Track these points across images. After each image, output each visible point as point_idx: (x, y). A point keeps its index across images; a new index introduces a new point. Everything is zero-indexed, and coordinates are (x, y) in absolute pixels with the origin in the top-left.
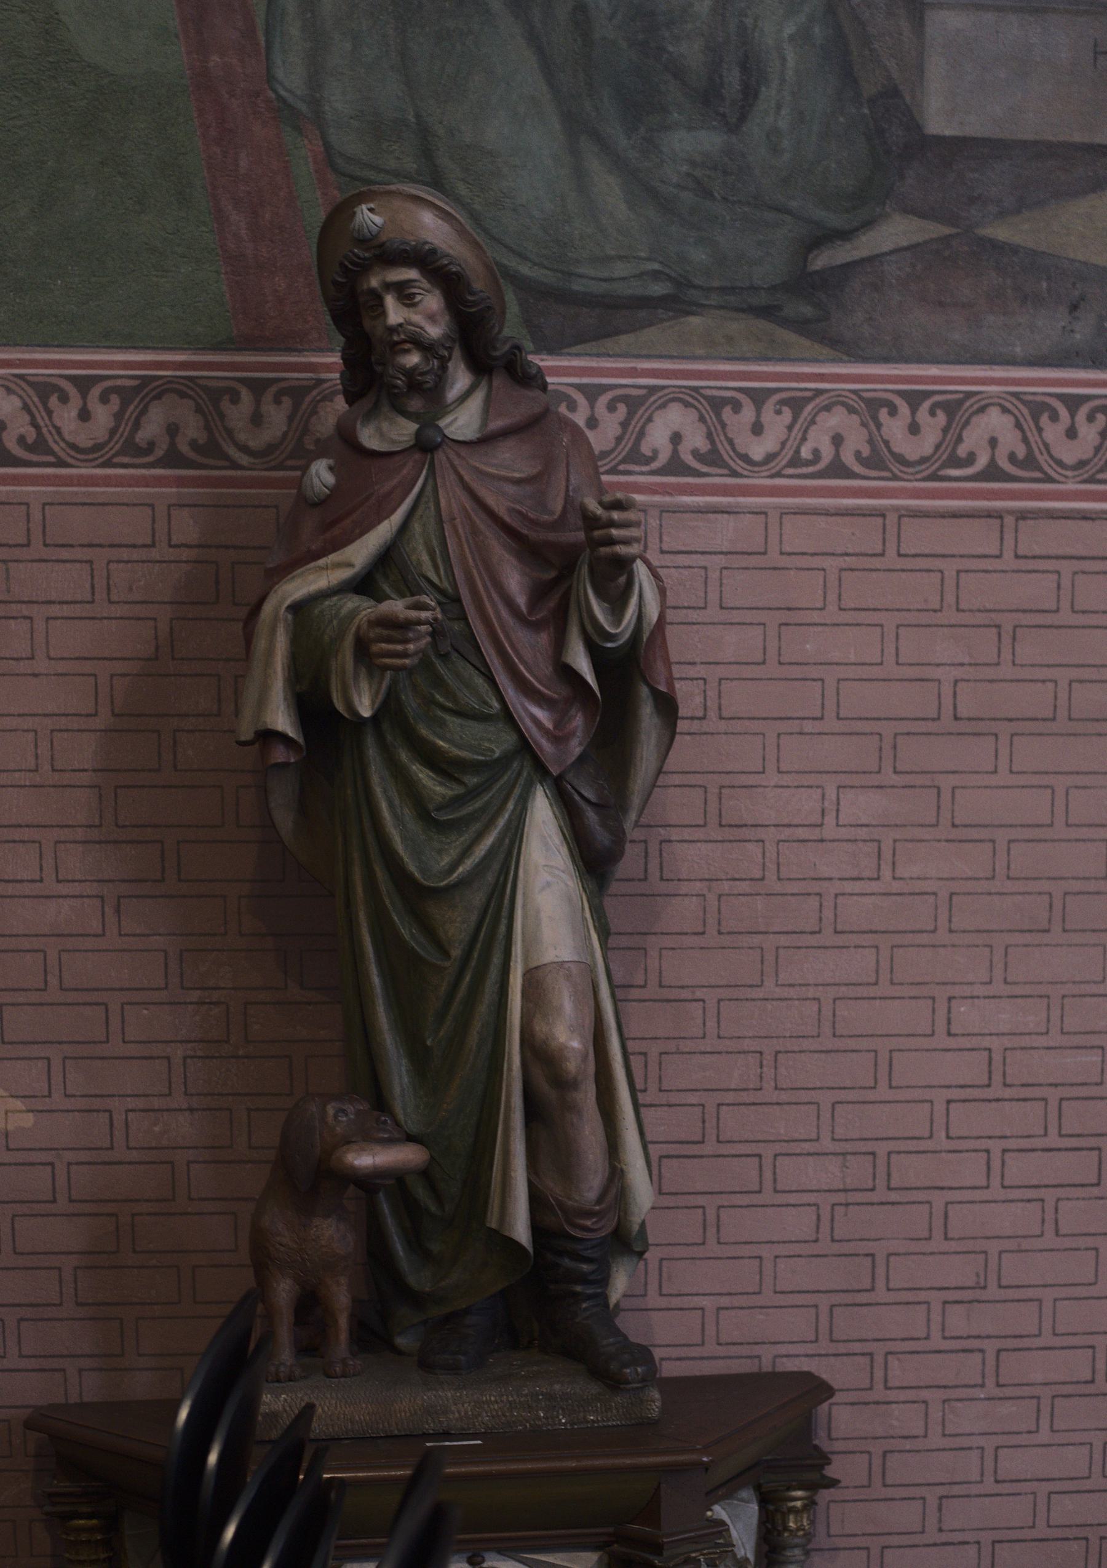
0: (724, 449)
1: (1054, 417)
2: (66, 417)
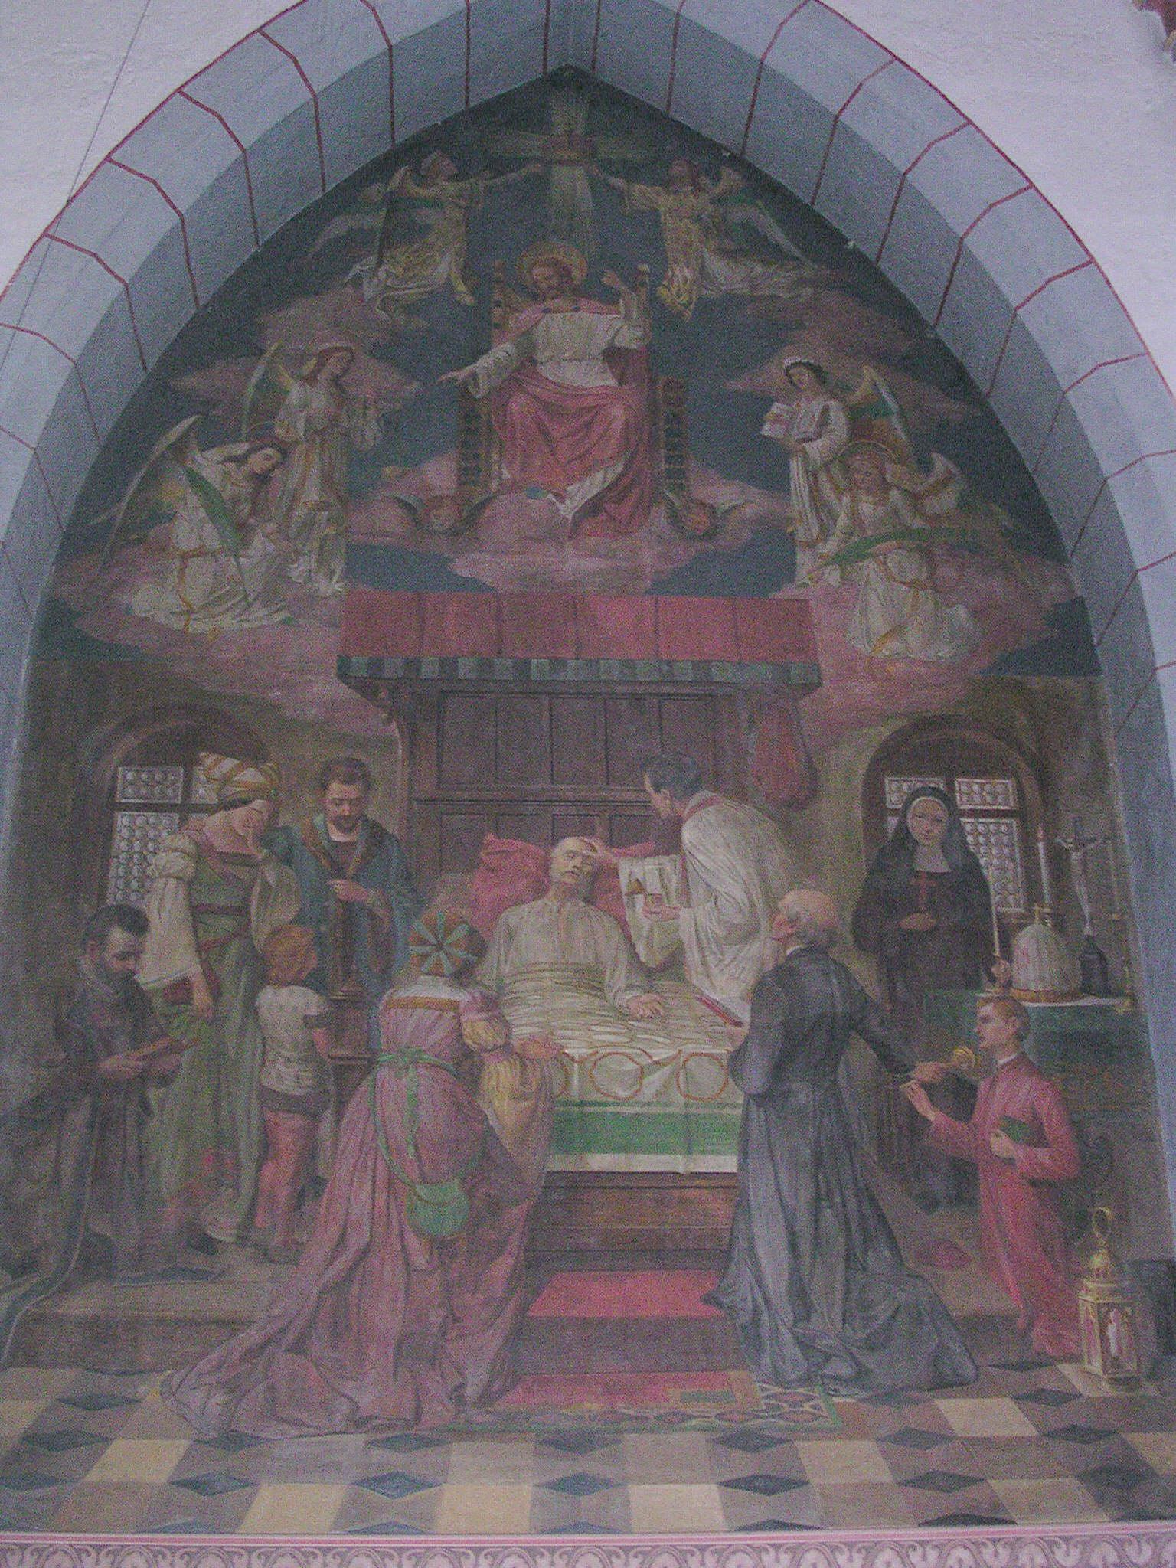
1: (164, 1556)
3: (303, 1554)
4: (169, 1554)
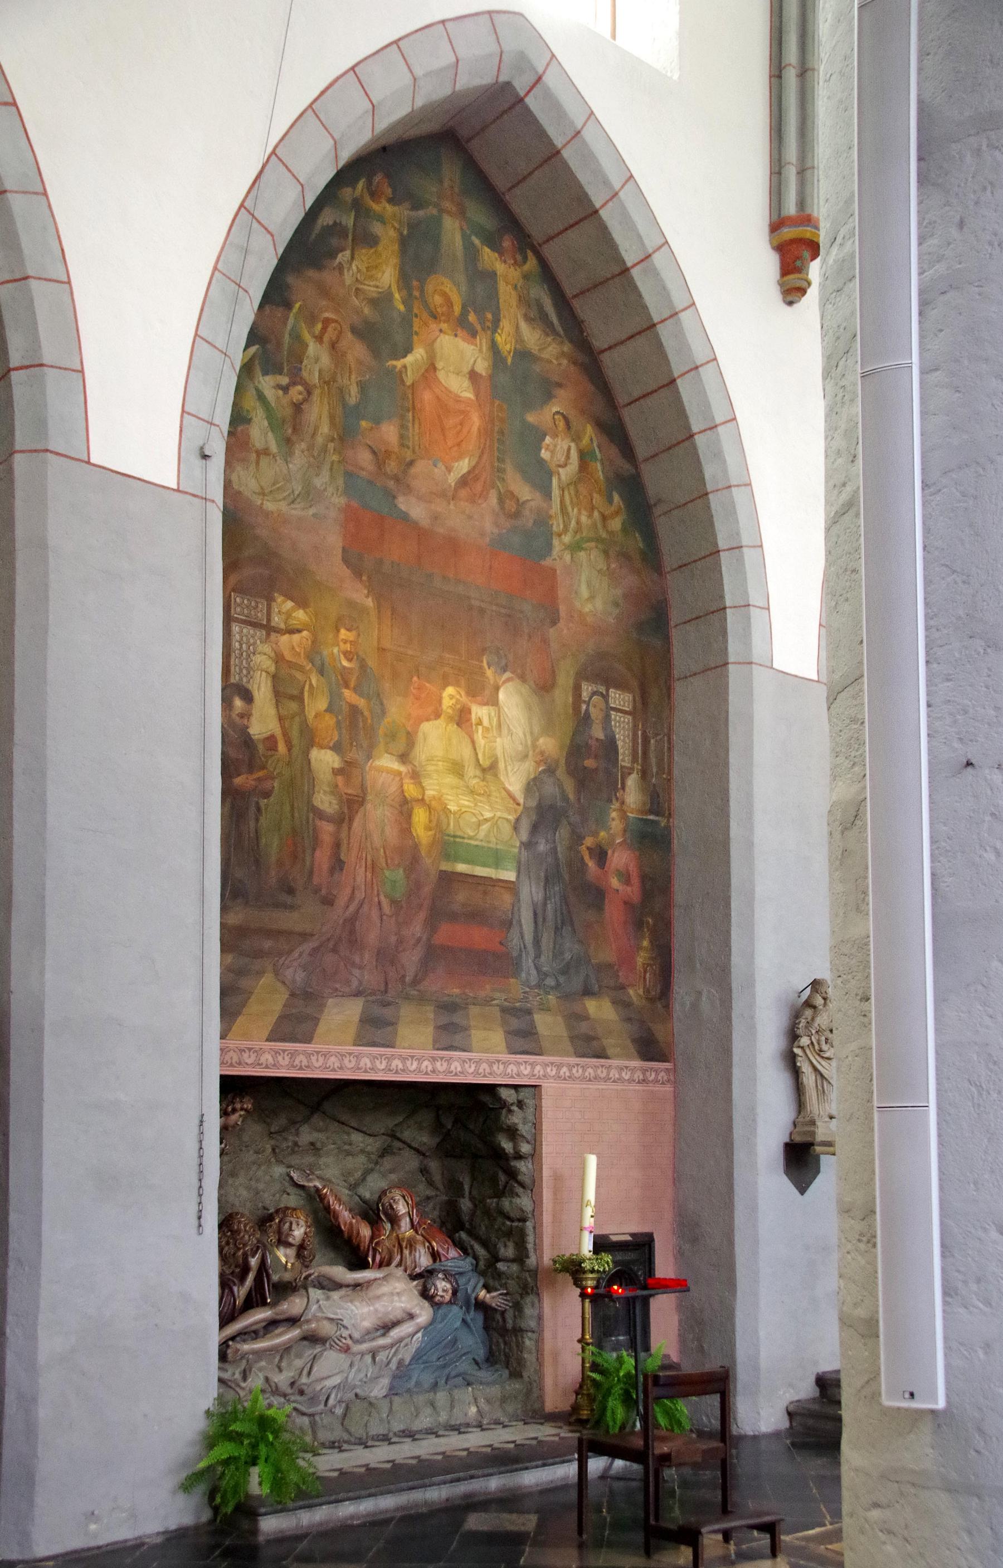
1: (280, 1054)
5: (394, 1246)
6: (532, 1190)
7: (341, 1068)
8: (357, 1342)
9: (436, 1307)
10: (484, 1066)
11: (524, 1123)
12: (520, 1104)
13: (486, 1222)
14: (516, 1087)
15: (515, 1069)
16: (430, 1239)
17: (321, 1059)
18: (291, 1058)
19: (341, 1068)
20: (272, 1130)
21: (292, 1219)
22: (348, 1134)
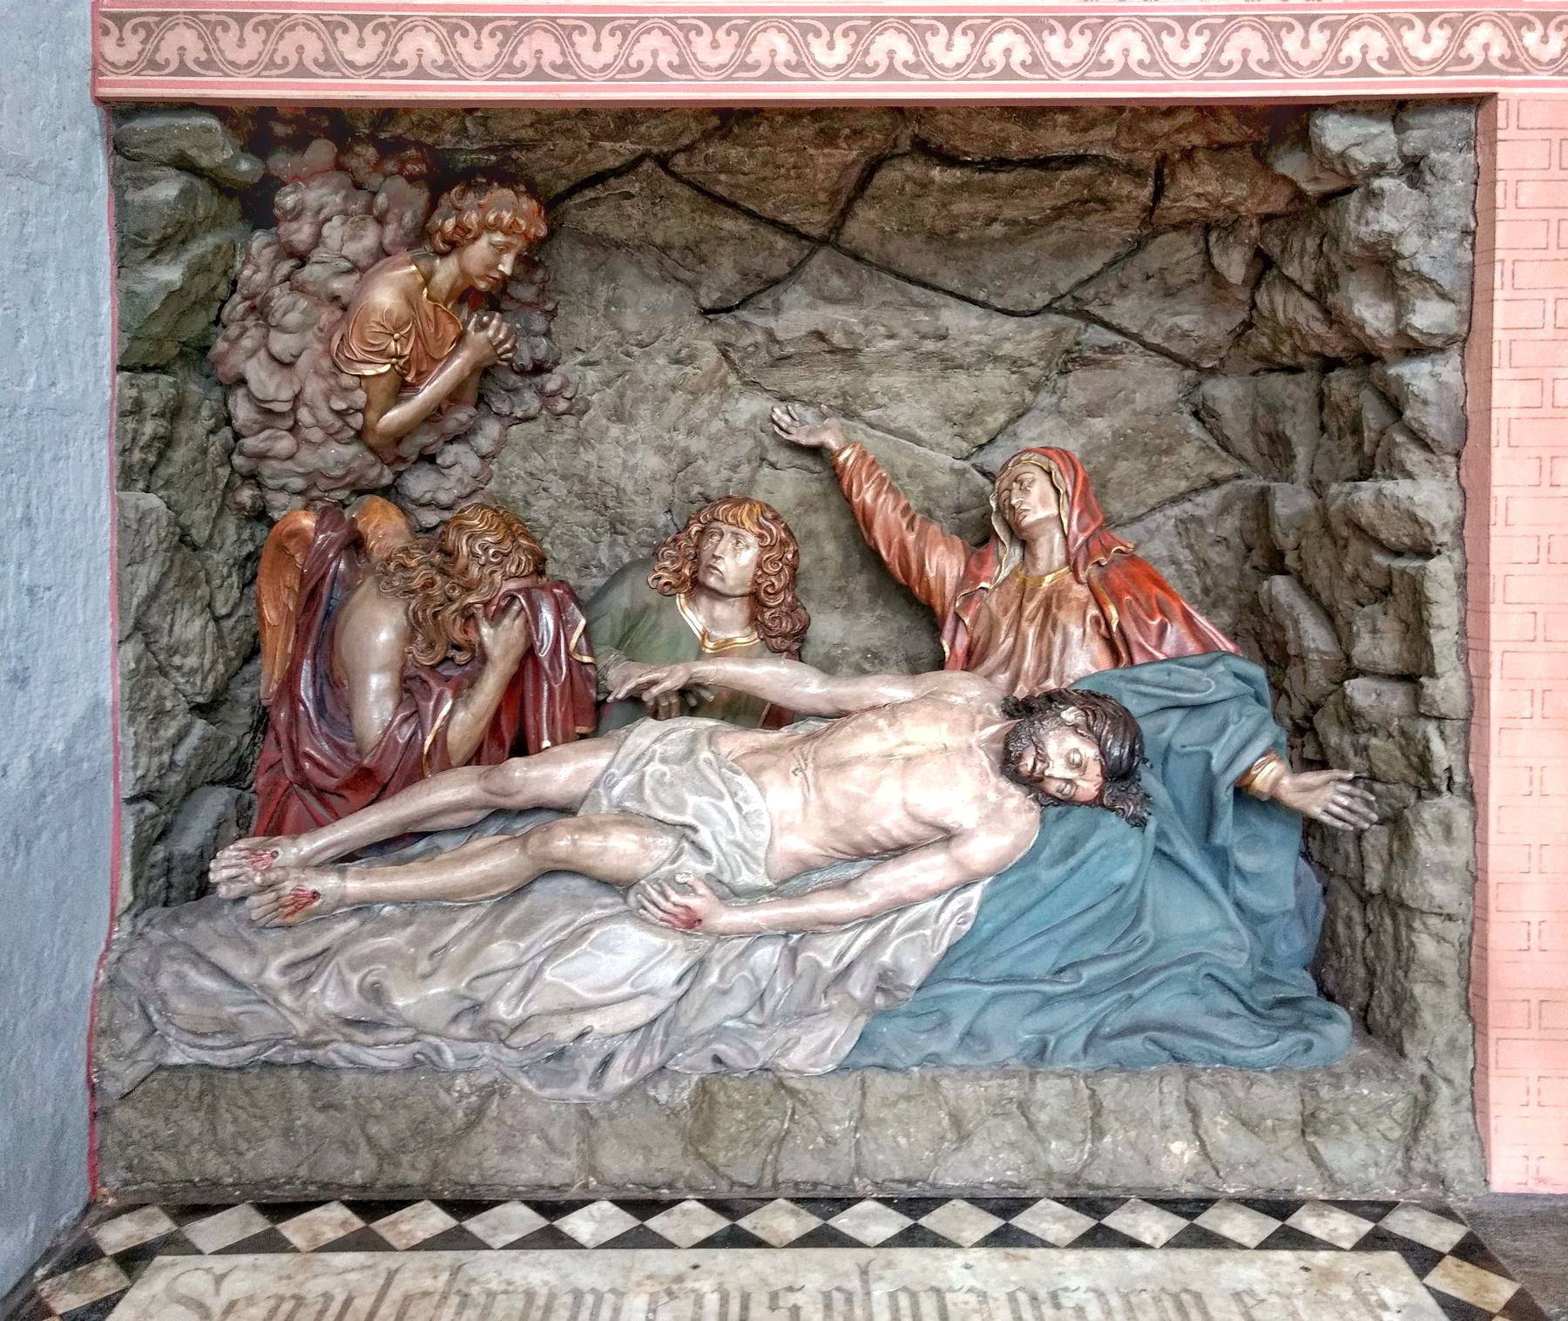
0: (690, 61)
1: (465, 34)
2: (313, 48)
3: (681, 27)
4: (234, 25)
5: (1006, 611)
6: (1458, 455)
7: (682, 68)
8: (732, 895)
9: (1053, 811)
10: (1248, 39)
11: (1428, 232)
12: (1414, 168)
13: (1330, 554)
14: (1398, 109)
15: (1379, 44)
16: (1105, 596)
17: (610, 44)
18: (502, 45)
19: (682, 68)
20: (707, 303)
21: (725, 527)
22: (927, 307)
